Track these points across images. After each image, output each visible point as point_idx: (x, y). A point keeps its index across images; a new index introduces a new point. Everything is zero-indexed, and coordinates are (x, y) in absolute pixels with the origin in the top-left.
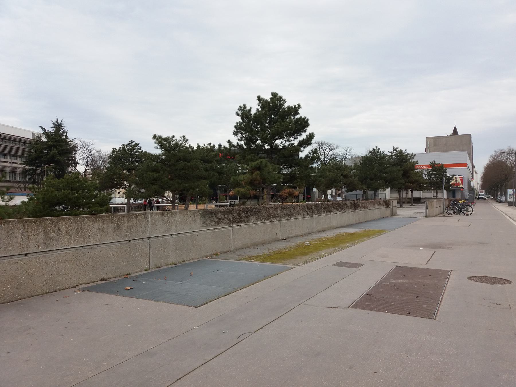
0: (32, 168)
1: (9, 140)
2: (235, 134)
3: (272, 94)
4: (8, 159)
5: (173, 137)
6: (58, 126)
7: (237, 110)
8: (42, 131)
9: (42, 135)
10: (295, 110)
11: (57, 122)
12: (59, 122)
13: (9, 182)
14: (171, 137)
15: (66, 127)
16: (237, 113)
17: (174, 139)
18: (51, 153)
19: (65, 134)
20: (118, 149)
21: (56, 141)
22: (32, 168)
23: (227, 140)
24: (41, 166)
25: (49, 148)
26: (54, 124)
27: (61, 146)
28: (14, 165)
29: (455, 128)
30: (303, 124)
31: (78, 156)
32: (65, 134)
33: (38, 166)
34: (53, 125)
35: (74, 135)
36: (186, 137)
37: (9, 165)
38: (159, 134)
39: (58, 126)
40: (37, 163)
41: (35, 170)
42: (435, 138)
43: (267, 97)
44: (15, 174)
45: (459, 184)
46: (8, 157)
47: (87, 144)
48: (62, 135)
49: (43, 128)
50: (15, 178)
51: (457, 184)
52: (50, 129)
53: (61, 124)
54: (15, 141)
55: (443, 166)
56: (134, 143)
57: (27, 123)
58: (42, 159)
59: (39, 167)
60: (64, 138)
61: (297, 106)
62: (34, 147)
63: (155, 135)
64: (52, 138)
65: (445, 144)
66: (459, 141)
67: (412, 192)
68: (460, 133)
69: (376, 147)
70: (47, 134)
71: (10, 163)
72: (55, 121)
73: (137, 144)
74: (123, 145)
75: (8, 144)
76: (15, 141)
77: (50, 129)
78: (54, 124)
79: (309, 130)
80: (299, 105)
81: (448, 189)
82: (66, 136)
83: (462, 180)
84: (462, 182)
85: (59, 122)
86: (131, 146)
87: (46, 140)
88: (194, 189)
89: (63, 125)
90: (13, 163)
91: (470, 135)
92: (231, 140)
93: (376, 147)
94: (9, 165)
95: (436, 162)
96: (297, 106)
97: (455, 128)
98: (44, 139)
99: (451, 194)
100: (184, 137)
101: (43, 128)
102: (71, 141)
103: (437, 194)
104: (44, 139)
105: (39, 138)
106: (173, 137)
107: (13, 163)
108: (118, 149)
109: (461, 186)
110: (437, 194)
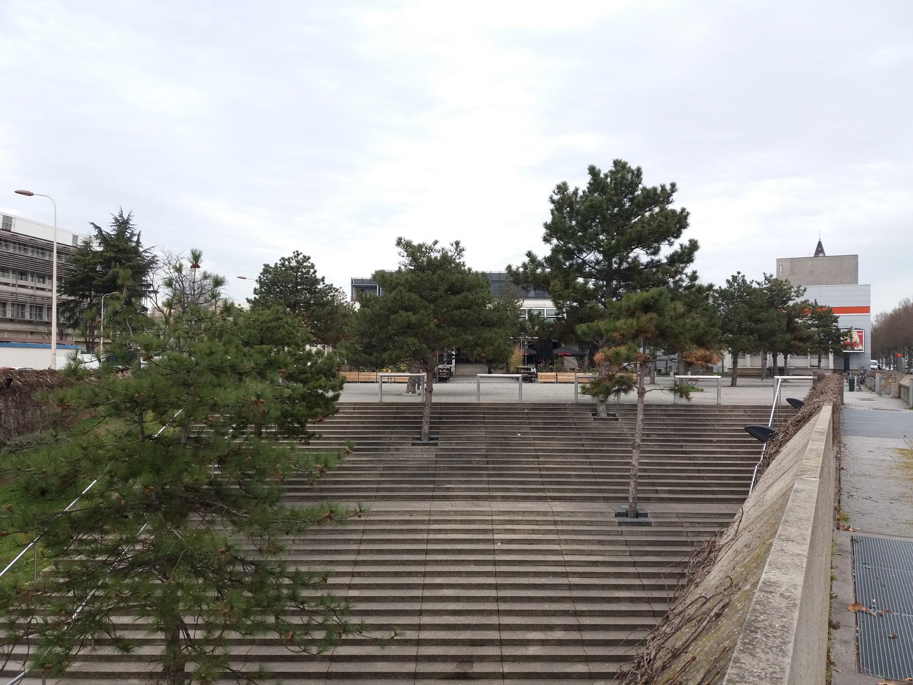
0: (73, 298)
1: (32, 247)
2: (546, 240)
3: (616, 163)
4: (29, 282)
5: (436, 243)
6: (123, 224)
7: (551, 193)
8: (96, 233)
9: (93, 238)
10: (662, 196)
11: (121, 216)
12: (125, 217)
13: (30, 322)
14: (429, 243)
15: (137, 225)
16: (551, 198)
17: (438, 247)
18: (111, 272)
19: (135, 239)
20: (273, 265)
21: (120, 251)
22: (73, 298)
23: (526, 252)
24: (90, 296)
25: (107, 262)
26: (116, 219)
27: (129, 260)
28: (39, 293)
29: (820, 244)
30: (680, 221)
31: (156, 277)
32: (135, 239)
33: (84, 296)
34: (113, 221)
35: (152, 239)
36: (461, 245)
37: (30, 292)
38: (407, 237)
39: (123, 224)
40: (83, 290)
41: (77, 303)
42: (793, 260)
43: (605, 168)
44: (23, 306)
45: (855, 344)
46: (30, 278)
47: (174, 257)
48: (130, 239)
49: (96, 227)
50: (41, 316)
51: (853, 345)
52: (109, 229)
53: (128, 219)
54: (42, 249)
55: (830, 310)
56: (301, 256)
57: (66, 219)
58: (95, 282)
59: (87, 297)
60: (134, 244)
61: (668, 187)
62: (78, 260)
63: (400, 239)
64: (114, 245)
65: (811, 272)
66: (846, 268)
67: (786, 358)
68: (828, 251)
69: (739, 273)
70: (103, 238)
71: (32, 288)
72: (117, 215)
73: (307, 259)
74: (283, 258)
75: (30, 254)
76: (42, 249)
77: (109, 229)
78: (116, 219)
79: (684, 239)
80: (673, 185)
81: (837, 353)
82: (138, 242)
83: (861, 337)
84: (861, 341)
85: (125, 217)
86: (297, 262)
87: (101, 249)
88: (483, 347)
89: (131, 222)
90: (37, 288)
91: (856, 257)
92: (535, 252)
93: (739, 273)
94: (30, 292)
95: (819, 304)
96: (668, 187)
97: (820, 244)
98: (97, 247)
99: (842, 361)
100: (457, 243)
101: (96, 227)
102: (145, 251)
103: (819, 361)
104: (97, 247)
105: (87, 244)
106: (436, 243)
107: (37, 288)
108: (273, 265)
109: (860, 347)
110: (819, 361)
